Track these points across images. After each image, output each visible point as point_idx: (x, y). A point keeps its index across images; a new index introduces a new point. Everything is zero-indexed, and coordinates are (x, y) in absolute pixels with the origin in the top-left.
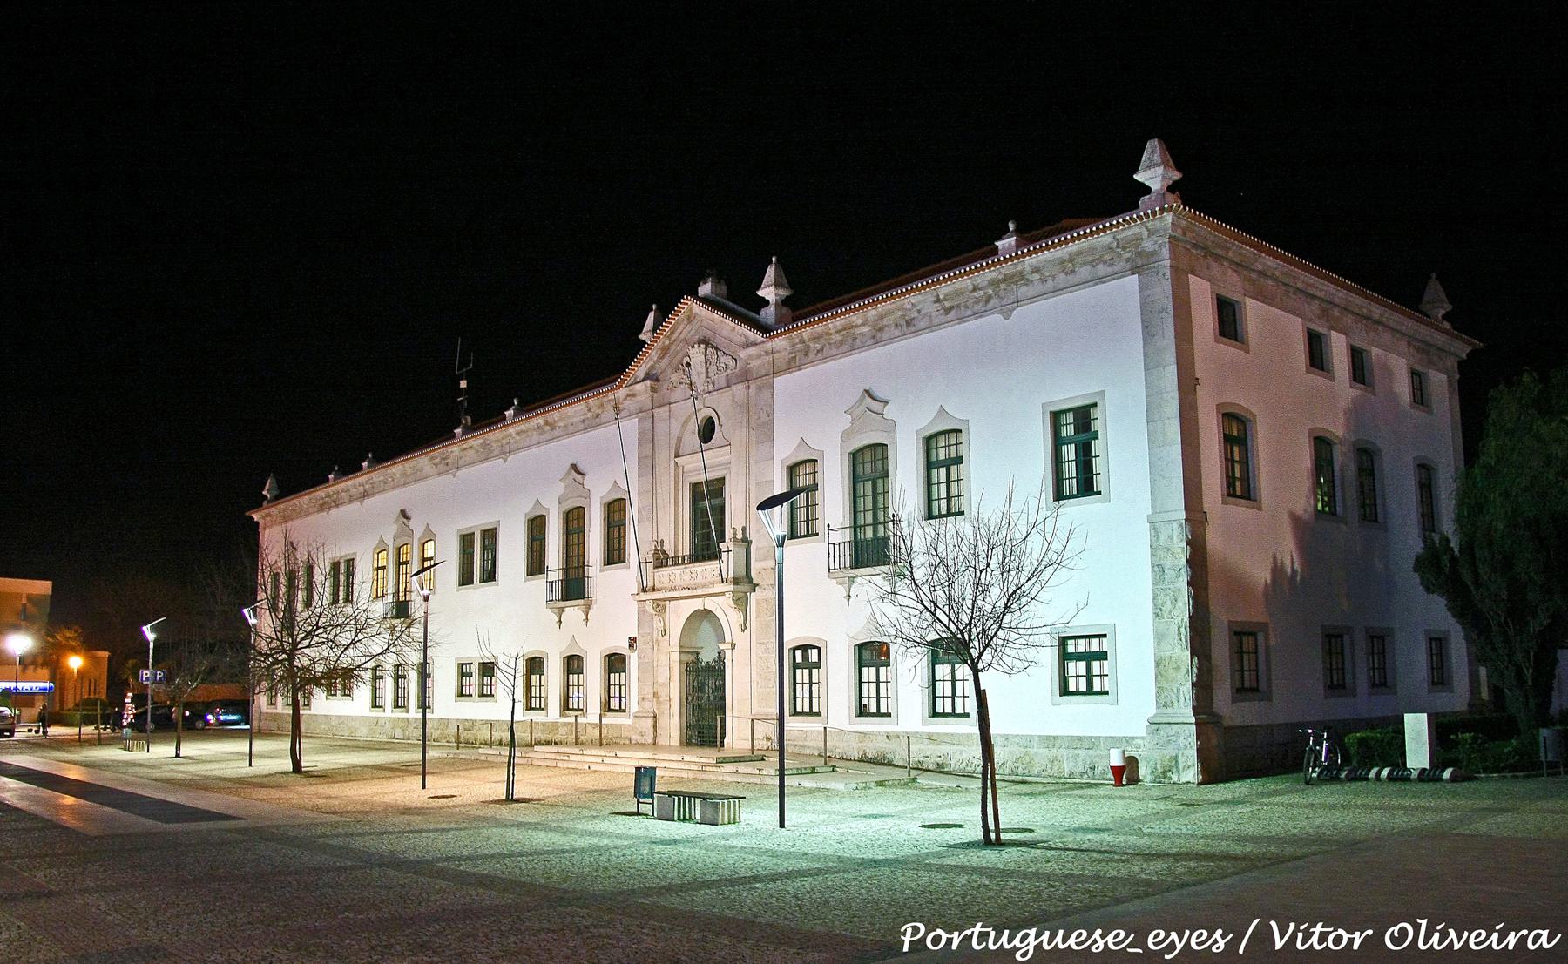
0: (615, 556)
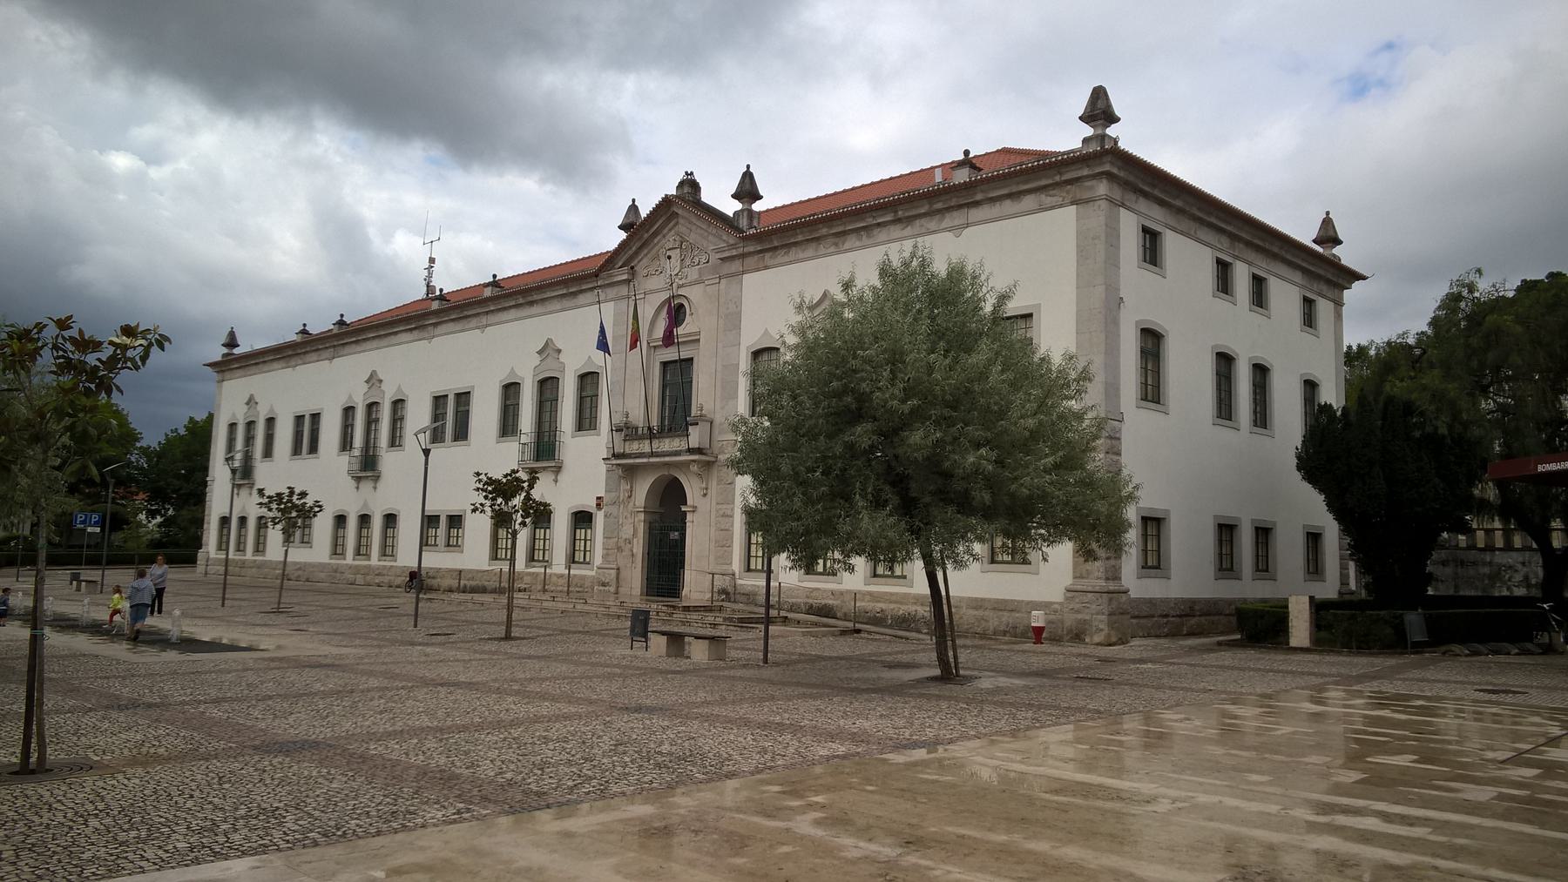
0: (585, 421)
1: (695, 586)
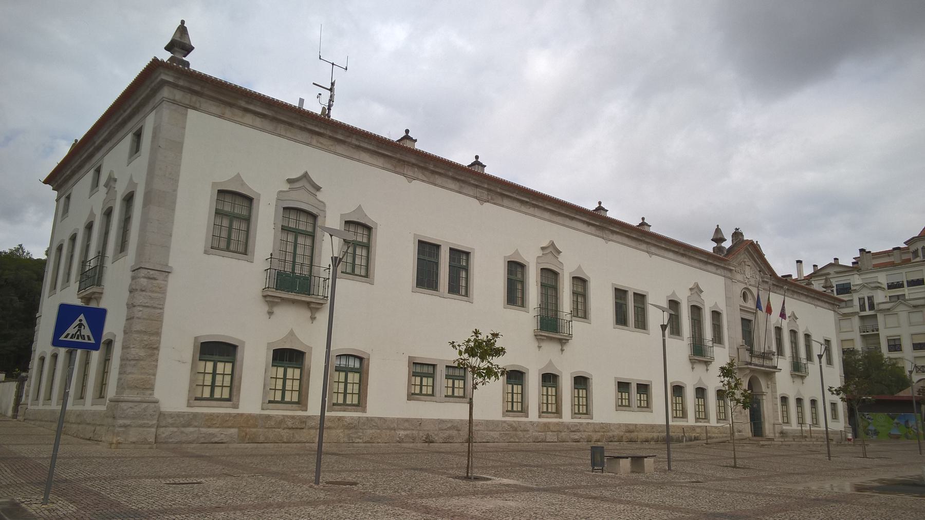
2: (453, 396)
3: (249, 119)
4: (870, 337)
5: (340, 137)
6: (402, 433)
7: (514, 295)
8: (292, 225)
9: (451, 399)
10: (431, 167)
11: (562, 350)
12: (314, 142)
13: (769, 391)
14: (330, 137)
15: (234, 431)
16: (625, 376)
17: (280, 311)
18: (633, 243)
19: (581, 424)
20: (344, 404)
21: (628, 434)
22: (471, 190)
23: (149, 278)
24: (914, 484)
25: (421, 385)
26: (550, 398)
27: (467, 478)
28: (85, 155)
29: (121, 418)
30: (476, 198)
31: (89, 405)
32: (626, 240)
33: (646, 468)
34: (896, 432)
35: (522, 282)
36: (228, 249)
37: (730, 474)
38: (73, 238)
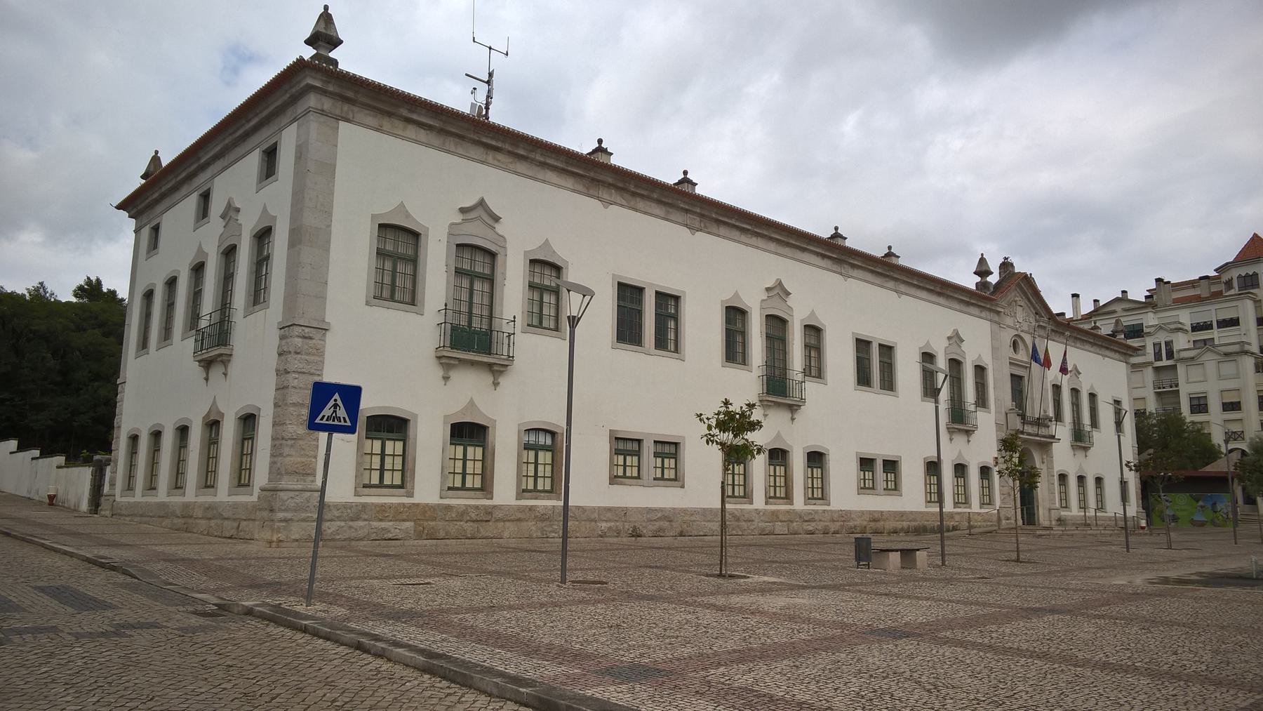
1: (1042, 515)
2: (662, 479)
3: (411, 131)
4: (1168, 394)
5: (522, 152)
6: (604, 525)
7: (735, 351)
8: (466, 266)
9: (661, 483)
10: (404, 112)
11: (793, 419)
12: (490, 159)
13: (1044, 467)
14: (509, 152)
15: (409, 524)
16: (630, 427)
17: (456, 375)
18: (878, 280)
19: (816, 512)
20: (535, 489)
21: (872, 524)
22: (677, 216)
23: (304, 337)
24: (1241, 577)
25: (625, 466)
26: (736, 477)
27: (720, 575)
28: (183, 175)
29: (281, 510)
30: (686, 226)
31: (223, 493)
32: (870, 277)
33: (919, 564)
34: (1199, 517)
35: (743, 334)
36: (392, 298)
37: (1018, 569)
38: (172, 283)
